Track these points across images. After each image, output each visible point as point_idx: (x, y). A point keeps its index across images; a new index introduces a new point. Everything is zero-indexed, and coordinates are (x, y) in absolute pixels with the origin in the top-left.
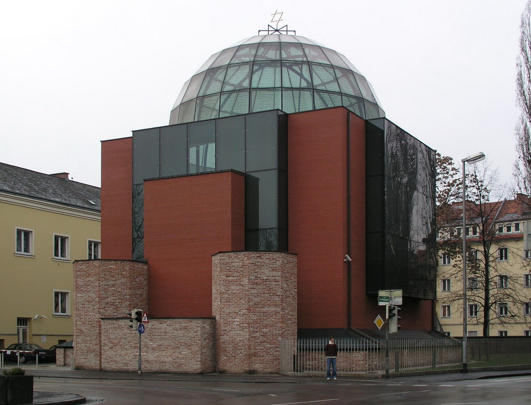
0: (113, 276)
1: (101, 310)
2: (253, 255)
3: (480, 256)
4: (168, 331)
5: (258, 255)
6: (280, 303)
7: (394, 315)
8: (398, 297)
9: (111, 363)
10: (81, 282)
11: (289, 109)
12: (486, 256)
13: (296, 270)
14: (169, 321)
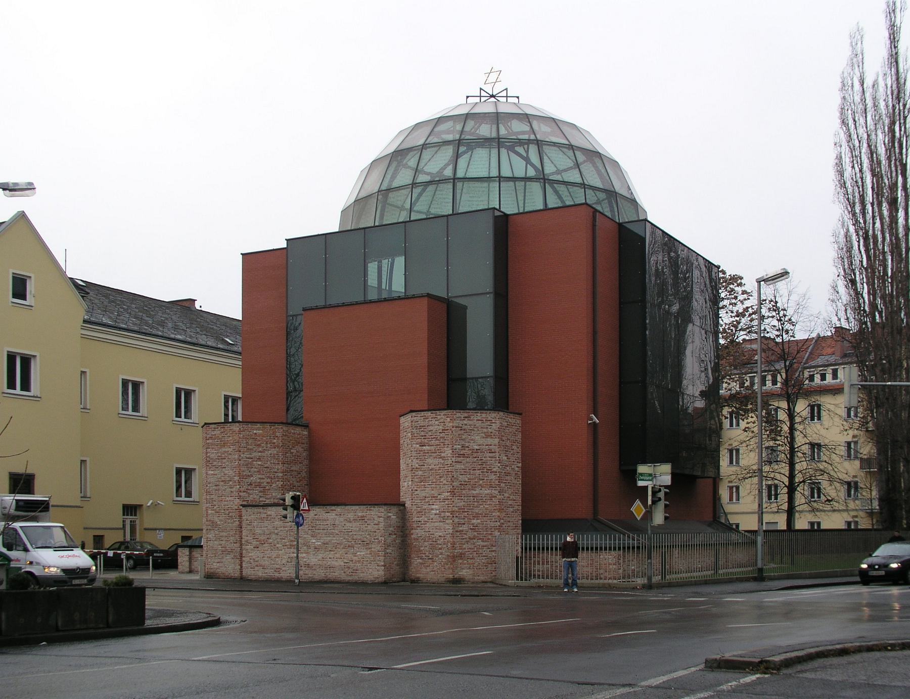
0: (259, 445)
1: (242, 494)
2: (458, 415)
3: (782, 416)
4: (337, 522)
5: (466, 415)
6: (497, 482)
7: (660, 499)
8: (665, 474)
9: (257, 568)
10: (213, 454)
11: (509, 208)
12: (791, 415)
13: (520, 436)
14: (339, 509)
